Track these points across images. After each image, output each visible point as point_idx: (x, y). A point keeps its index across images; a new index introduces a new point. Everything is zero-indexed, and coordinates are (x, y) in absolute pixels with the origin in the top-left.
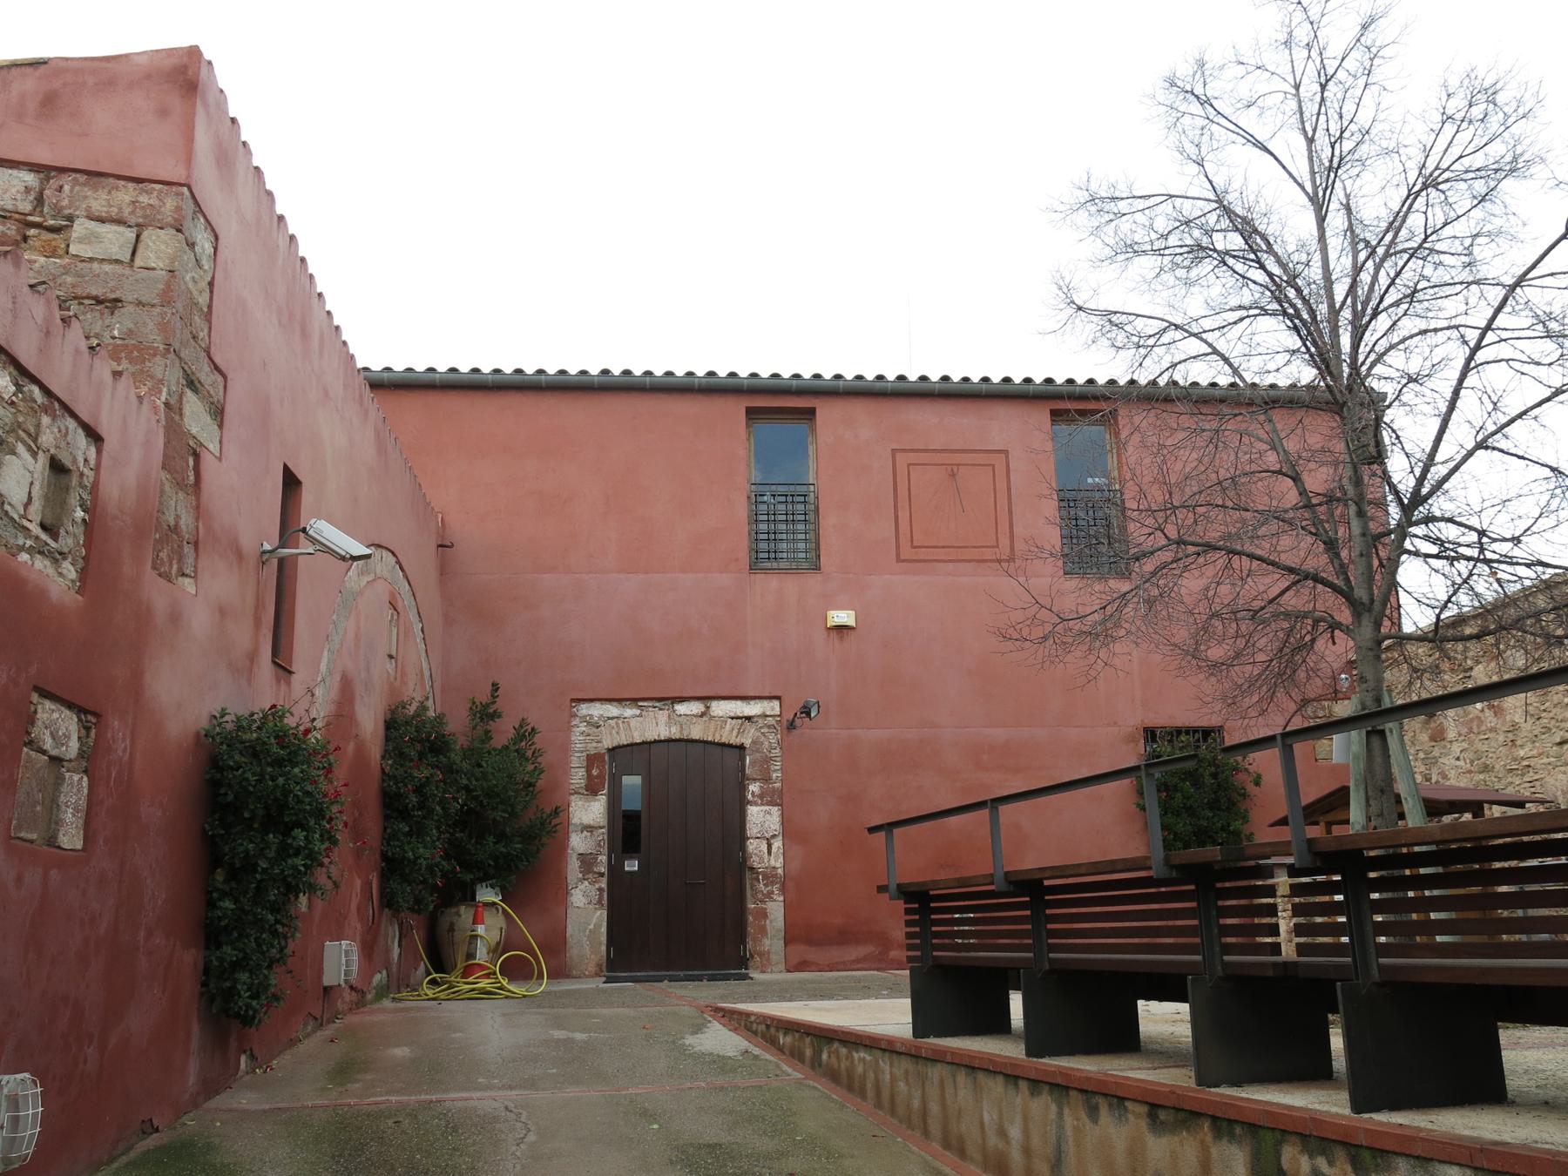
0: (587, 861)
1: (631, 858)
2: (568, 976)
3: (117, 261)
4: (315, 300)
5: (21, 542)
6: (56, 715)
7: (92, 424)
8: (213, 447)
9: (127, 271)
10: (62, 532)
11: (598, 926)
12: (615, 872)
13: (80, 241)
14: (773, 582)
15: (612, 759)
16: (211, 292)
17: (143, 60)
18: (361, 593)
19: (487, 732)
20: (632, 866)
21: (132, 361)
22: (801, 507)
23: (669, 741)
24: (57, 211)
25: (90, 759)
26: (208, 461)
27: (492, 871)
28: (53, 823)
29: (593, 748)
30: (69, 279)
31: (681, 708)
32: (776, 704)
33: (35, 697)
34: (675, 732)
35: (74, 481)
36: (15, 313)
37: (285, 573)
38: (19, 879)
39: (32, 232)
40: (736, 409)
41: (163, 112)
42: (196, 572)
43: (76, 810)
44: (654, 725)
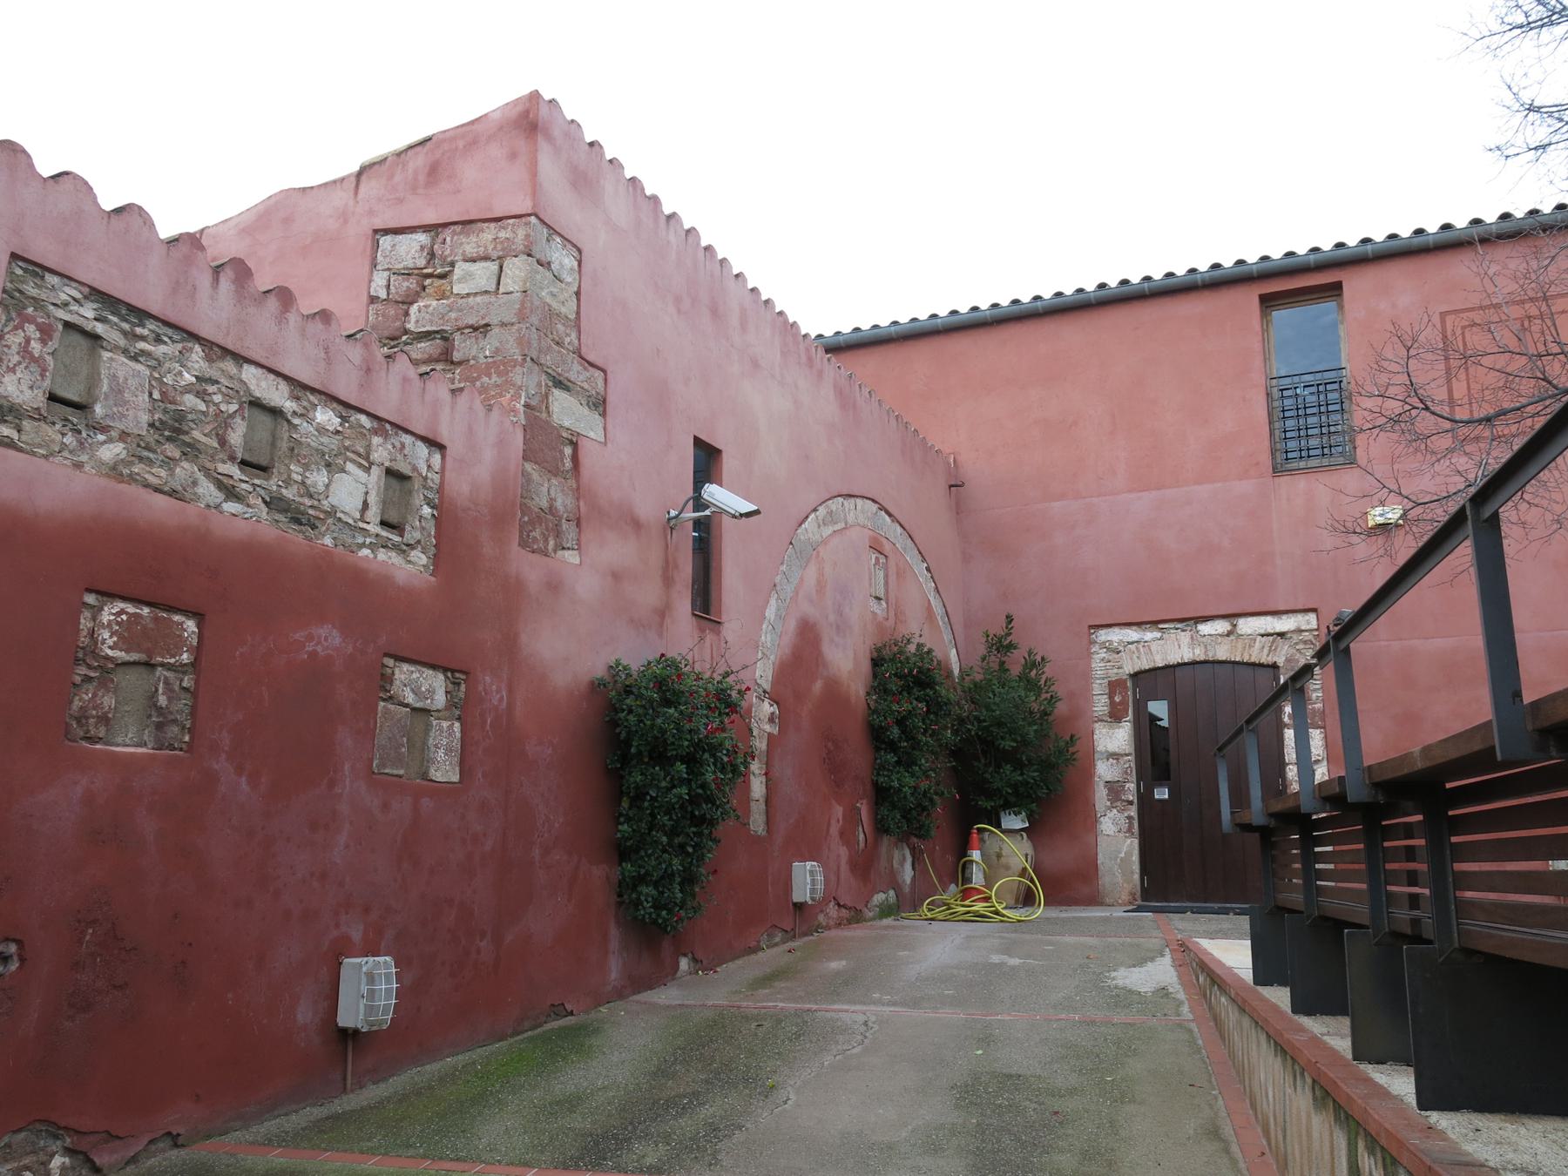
0: (1114, 789)
1: (1161, 785)
2: (1101, 904)
3: (486, 292)
4: (732, 283)
5: (360, 540)
6: (414, 676)
7: (430, 436)
8: (596, 434)
9: (493, 299)
10: (408, 528)
11: (1129, 854)
12: (1145, 800)
13: (460, 281)
14: (1301, 483)
15: (1135, 686)
16: (578, 300)
17: (497, 115)
18: (825, 542)
19: (1002, 663)
20: (1162, 794)
21: (499, 374)
22: (1336, 395)
23: (1194, 663)
24: (444, 263)
25: (461, 708)
26: (586, 448)
27: (1012, 799)
28: (425, 761)
29: (1114, 674)
30: (453, 315)
31: (1205, 628)
32: (1312, 617)
33: (390, 662)
34: (1199, 654)
35: (417, 484)
36: (329, 361)
37: (705, 536)
38: (386, 806)
39: (428, 282)
40: (1249, 298)
41: (513, 156)
42: (579, 544)
43: (448, 751)
44: (1176, 648)
